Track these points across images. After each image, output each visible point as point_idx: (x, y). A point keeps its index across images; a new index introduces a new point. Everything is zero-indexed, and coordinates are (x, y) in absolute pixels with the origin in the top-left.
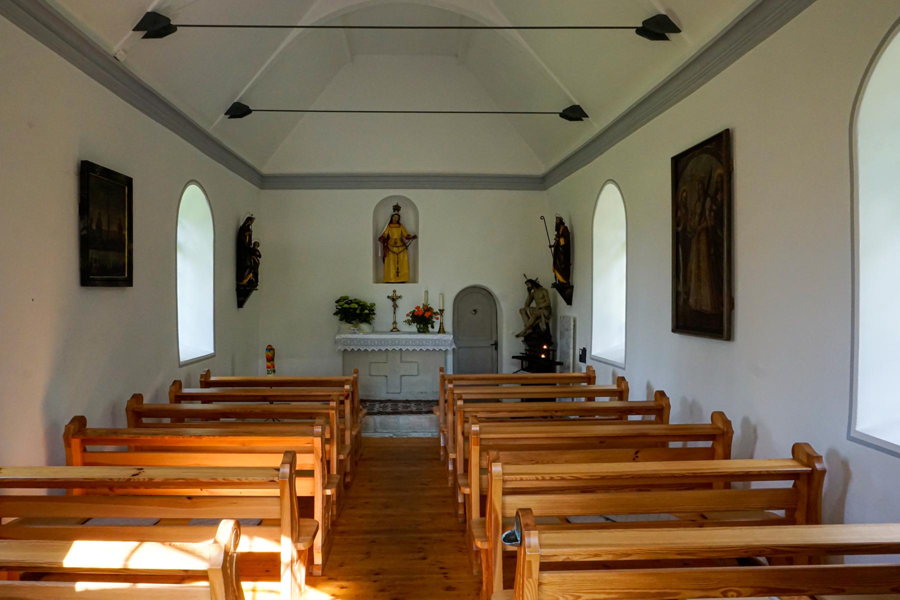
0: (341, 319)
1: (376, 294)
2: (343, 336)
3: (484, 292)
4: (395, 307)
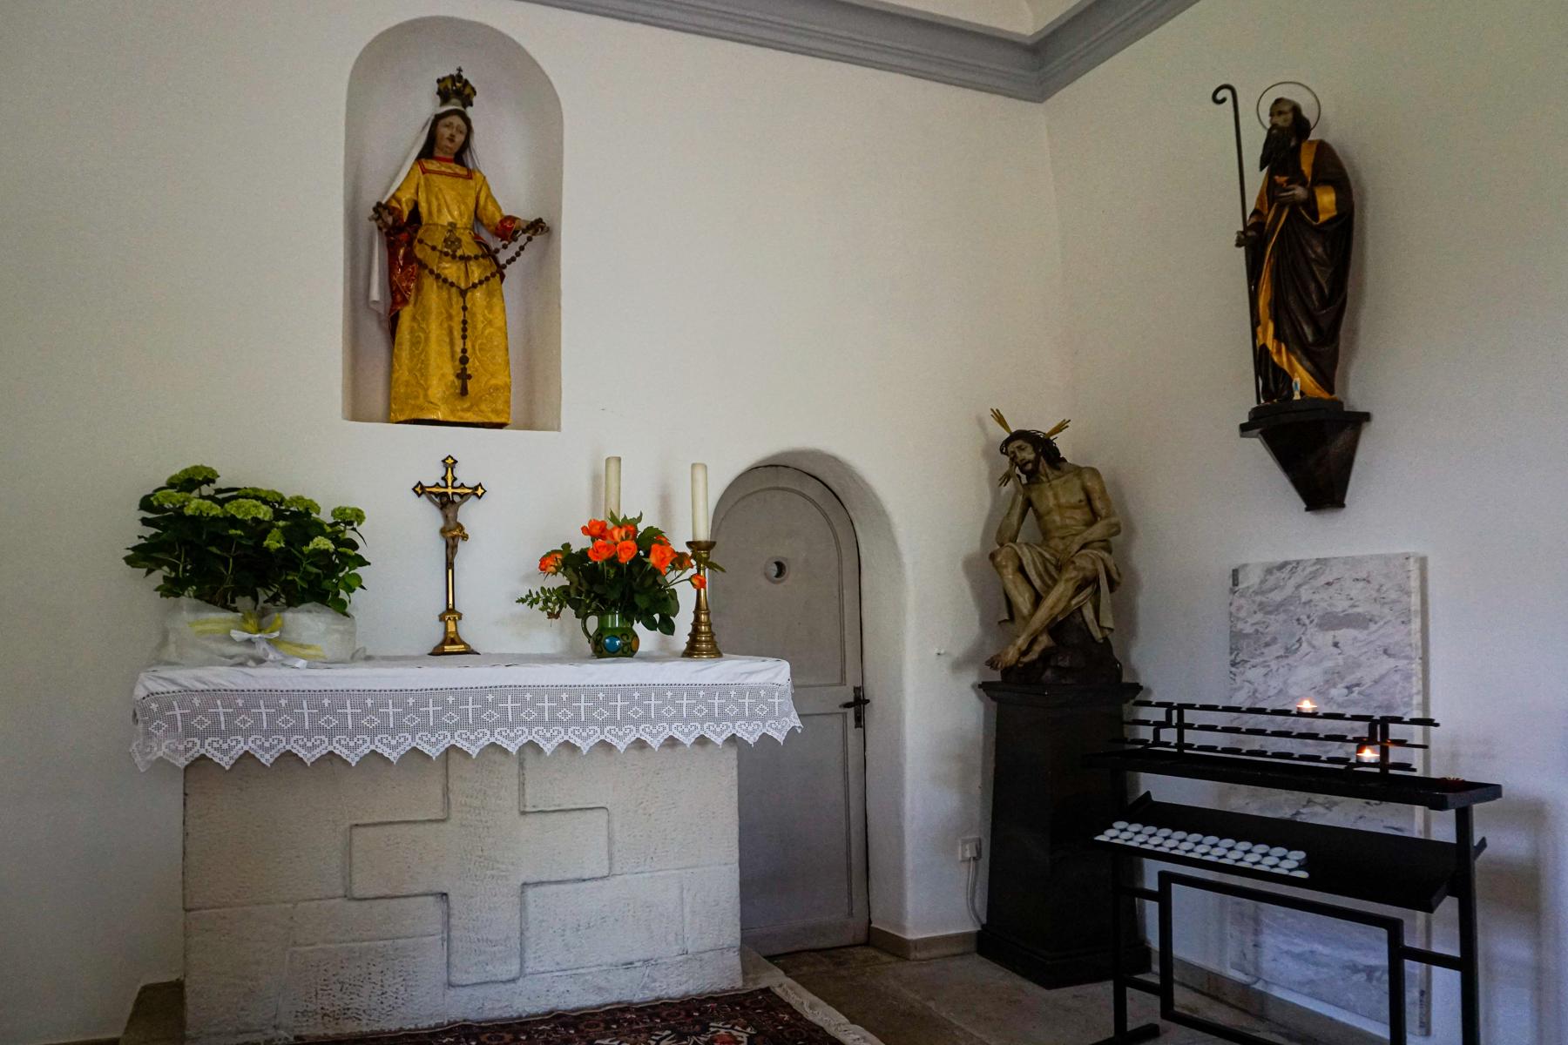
0: (172, 588)
1: (364, 471)
2: (186, 677)
4: (453, 536)
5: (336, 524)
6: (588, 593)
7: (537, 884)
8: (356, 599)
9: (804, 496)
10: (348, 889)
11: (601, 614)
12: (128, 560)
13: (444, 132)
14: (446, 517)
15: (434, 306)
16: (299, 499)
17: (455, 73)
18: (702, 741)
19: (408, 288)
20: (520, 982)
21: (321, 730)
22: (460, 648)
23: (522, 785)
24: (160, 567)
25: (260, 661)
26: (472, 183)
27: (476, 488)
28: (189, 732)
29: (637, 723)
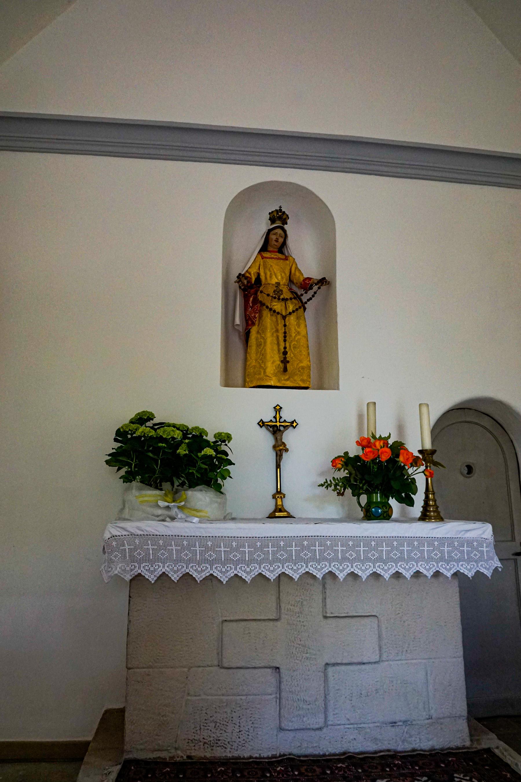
0: (128, 478)
1: (233, 414)
2: (131, 526)
3: (486, 422)
4: (280, 450)
5: (217, 442)
6: (361, 480)
7: (334, 665)
8: (227, 484)
9: (482, 426)
10: (220, 661)
11: (369, 493)
12: (108, 462)
13: (273, 237)
14: (276, 439)
15: (269, 325)
16: (197, 428)
17: (278, 209)
18: (437, 574)
19: (255, 317)
20: (325, 730)
21: (206, 561)
22: (285, 514)
23: (324, 599)
24: (125, 466)
25: (173, 519)
26: (288, 262)
27: (293, 422)
28: (133, 559)
29: (396, 561)
